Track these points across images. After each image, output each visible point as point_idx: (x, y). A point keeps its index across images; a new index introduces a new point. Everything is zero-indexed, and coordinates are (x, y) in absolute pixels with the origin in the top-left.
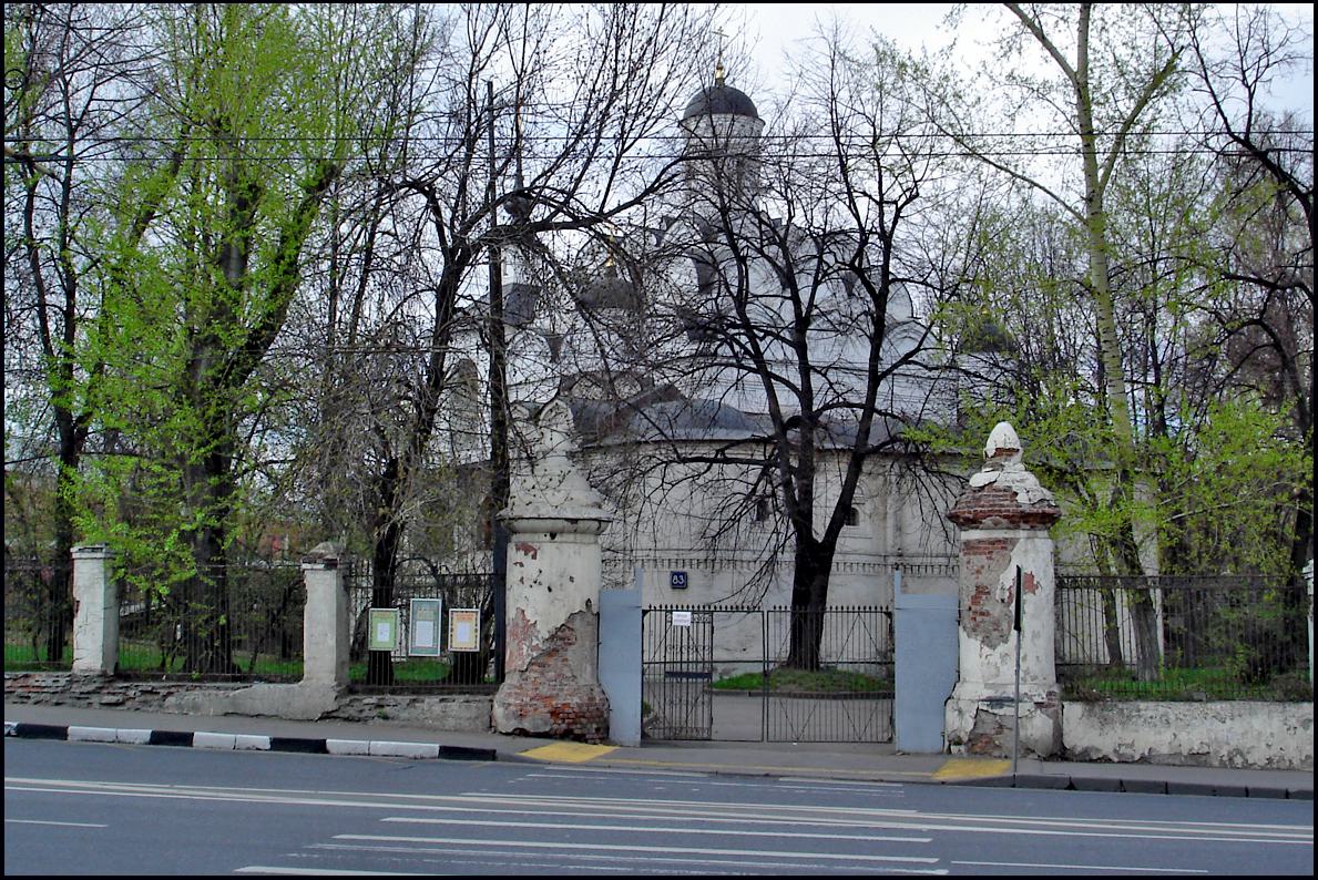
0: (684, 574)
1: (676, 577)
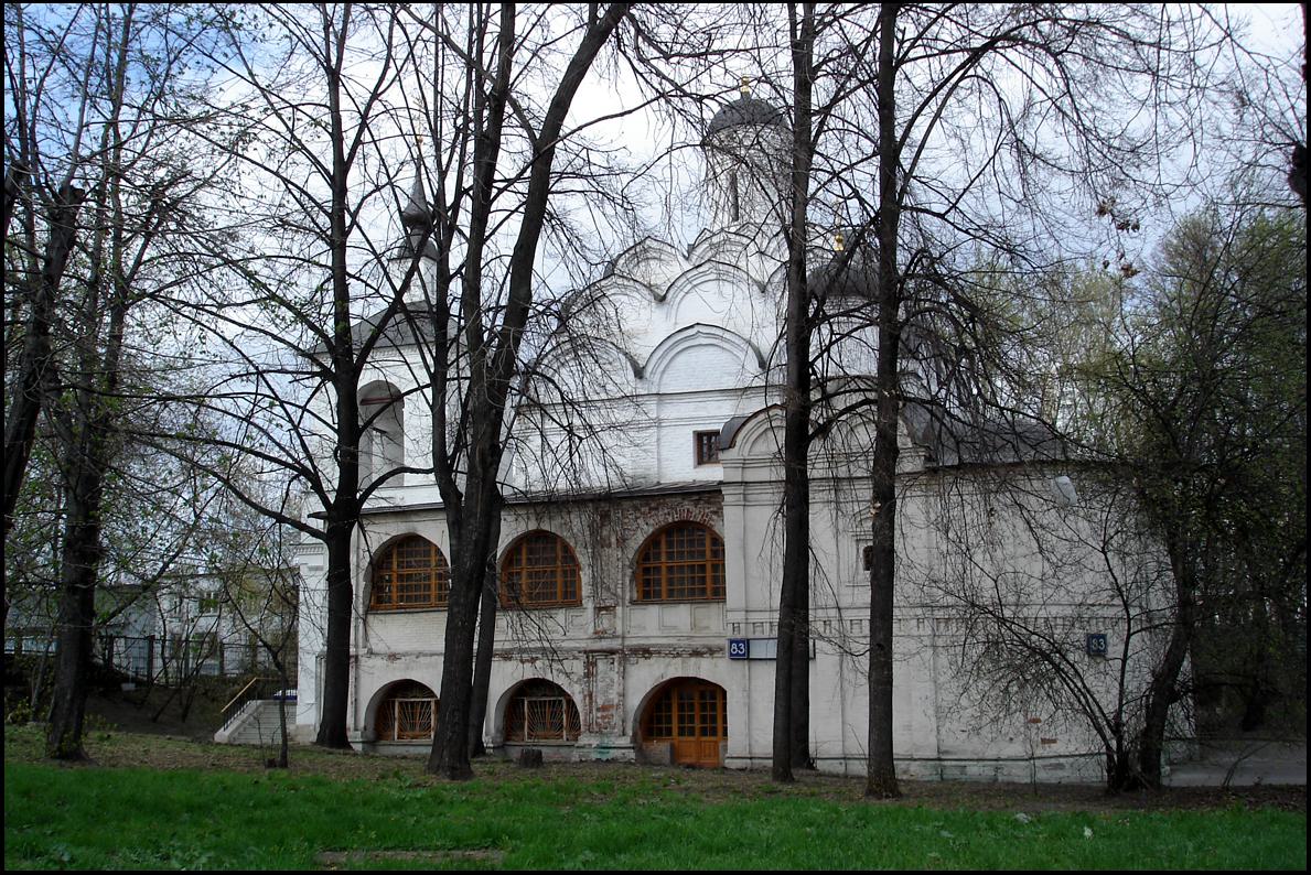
0: (1104, 637)
1: (734, 646)
